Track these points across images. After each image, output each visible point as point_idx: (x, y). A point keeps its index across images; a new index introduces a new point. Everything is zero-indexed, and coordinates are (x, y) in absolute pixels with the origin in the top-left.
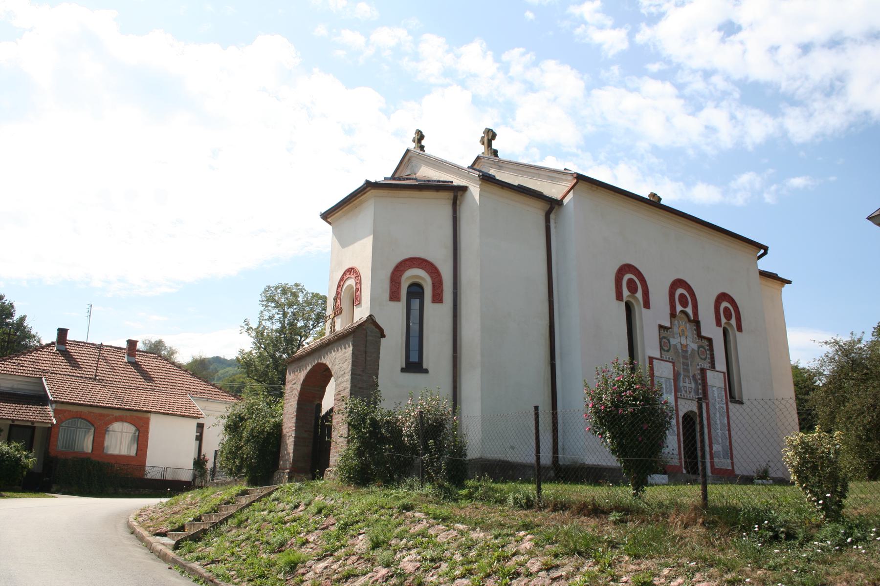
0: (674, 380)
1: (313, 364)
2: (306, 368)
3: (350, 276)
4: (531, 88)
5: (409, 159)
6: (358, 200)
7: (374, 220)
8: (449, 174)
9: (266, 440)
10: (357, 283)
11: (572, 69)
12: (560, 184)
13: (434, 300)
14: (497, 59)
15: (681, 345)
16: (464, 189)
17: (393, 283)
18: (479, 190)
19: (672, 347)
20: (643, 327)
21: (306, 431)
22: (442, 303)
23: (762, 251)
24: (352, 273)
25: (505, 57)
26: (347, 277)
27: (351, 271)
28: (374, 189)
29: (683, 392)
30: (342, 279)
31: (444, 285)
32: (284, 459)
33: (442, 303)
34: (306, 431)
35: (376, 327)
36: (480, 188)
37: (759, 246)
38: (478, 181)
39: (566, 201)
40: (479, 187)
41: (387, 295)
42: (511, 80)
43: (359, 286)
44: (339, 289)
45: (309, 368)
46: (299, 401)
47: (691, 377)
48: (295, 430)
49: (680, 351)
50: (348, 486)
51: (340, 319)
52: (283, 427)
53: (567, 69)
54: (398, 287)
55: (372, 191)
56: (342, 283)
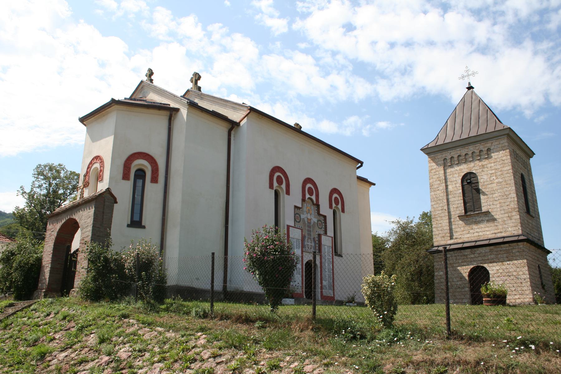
0: (301, 240)
1: (67, 219)
2: (61, 222)
6: (101, 114)
9: (30, 269)
10: (101, 167)
15: (307, 219)
16: (177, 110)
18: (187, 111)
19: (301, 220)
21: (59, 264)
22: (157, 183)
23: (360, 164)
29: (307, 248)
30: (91, 163)
32: (42, 282)
34: (59, 264)
37: (358, 161)
39: (242, 123)
41: (121, 176)
43: (102, 168)
44: (89, 169)
45: (63, 221)
46: (55, 243)
47: (312, 240)
49: (307, 223)
51: (88, 190)
52: (43, 261)
55: (116, 106)
56: (91, 166)
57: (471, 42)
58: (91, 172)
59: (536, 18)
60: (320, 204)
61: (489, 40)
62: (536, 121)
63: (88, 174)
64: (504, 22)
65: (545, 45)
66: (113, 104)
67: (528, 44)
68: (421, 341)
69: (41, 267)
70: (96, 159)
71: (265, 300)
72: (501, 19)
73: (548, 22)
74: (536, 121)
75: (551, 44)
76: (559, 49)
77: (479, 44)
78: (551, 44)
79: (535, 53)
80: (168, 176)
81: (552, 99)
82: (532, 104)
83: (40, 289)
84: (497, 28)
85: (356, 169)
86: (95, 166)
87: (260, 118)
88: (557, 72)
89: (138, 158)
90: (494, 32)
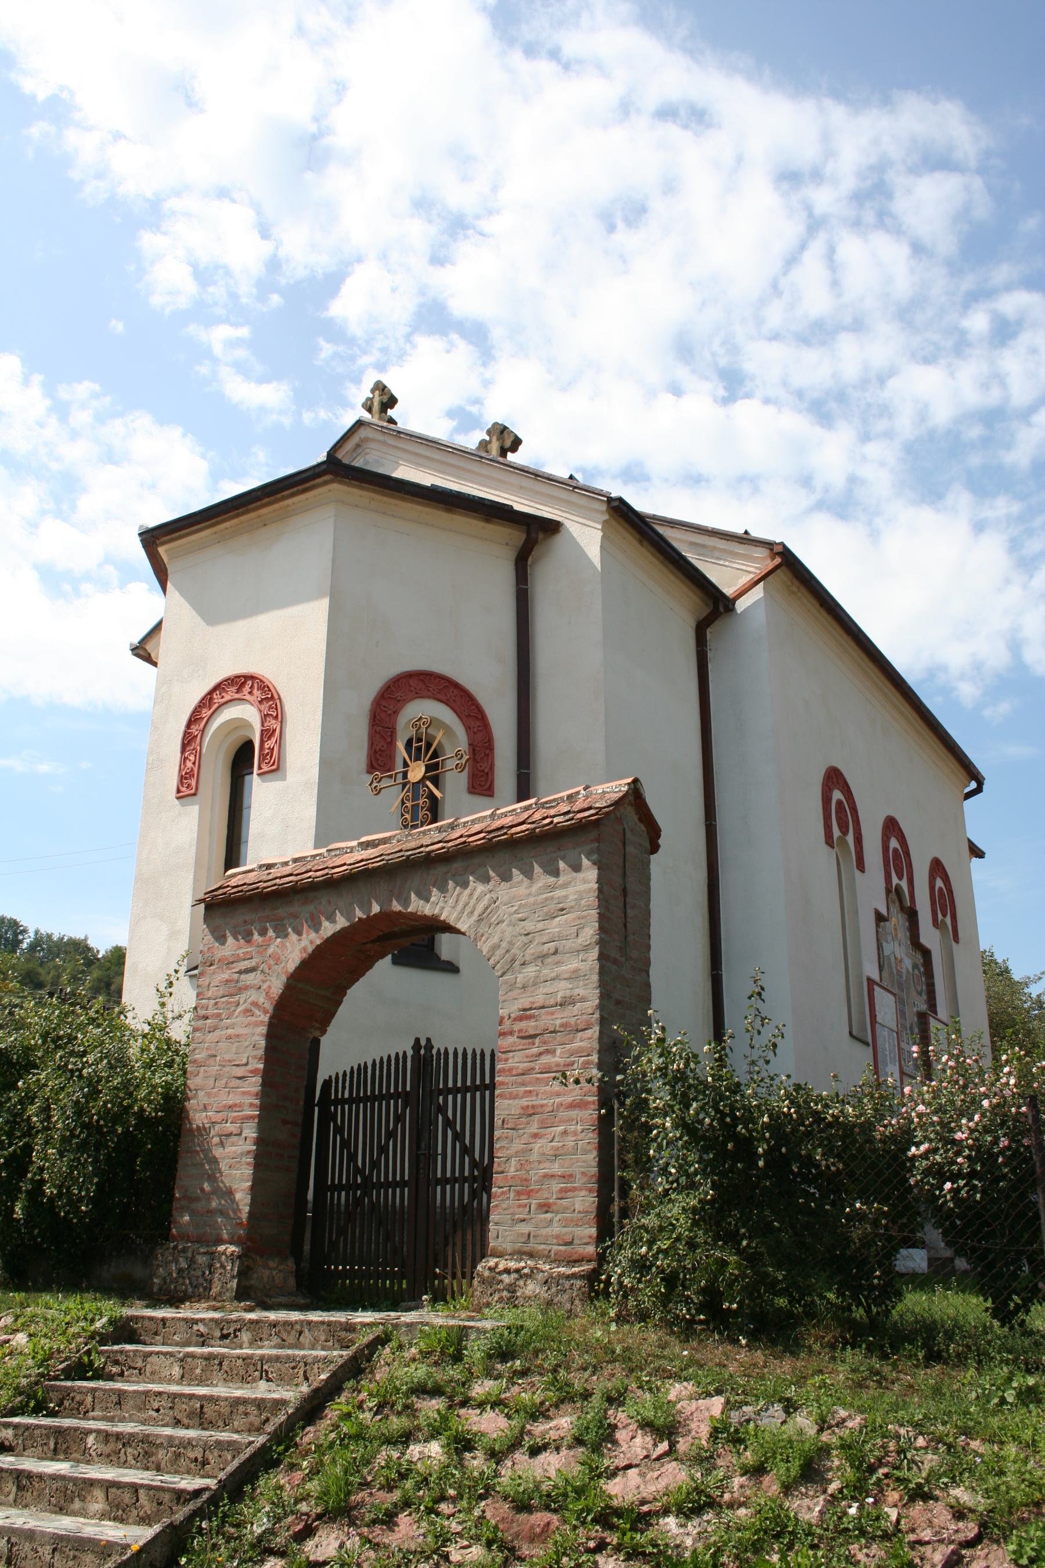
1: (359, 914)
2: (316, 927)
3: (237, 696)
4: (111, 457)
5: (358, 446)
6: (276, 506)
7: (334, 560)
8: (496, 489)
9: (129, 1144)
10: (264, 718)
11: (185, 435)
12: (727, 563)
13: (473, 787)
14: (49, 390)
16: (552, 527)
17: (378, 729)
18: (600, 534)
20: (857, 912)
21: (285, 1122)
22: (492, 796)
23: (973, 785)
24: (247, 689)
25: (64, 393)
26: (227, 697)
27: (244, 684)
28: (341, 483)
30: (207, 701)
31: (496, 751)
32: (199, 1206)
33: (492, 796)
34: (285, 1122)
35: (640, 820)
36: (602, 530)
37: (972, 773)
38: (602, 512)
39: (741, 605)
40: (600, 527)
41: (360, 756)
42: (75, 435)
43: (272, 723)
44: (195, 729)
45: (328, 929)
46: (271, 1025)
48: (259, 1116)
50: (833, 1359)
51: (196, 808)
52: (191, 1104)
53: (175, 432)
54: (389, 740)
55: (335, 486)
56: (206, 713)
57: (806, 481)
58: (207, 740)
59: (975, 432)
60: (918, 908)
61: (853, 480)
62: (987, 713)
63: (195, 744)
64: (889, 435)
65: (1002, 507)
66: (327, 477)
67: (961, 499)
68: (187, 1367)
69: (177, 1137)
70: (234, 689)
71: (746, 1267)
72: (881, 425)
73: (1009, 446)
74: (987, 713)
75: (1016, 508)
76: (1038, 522)
77: (826, 490)
78: (1016, 508)
79: (979, 527)
80: (531, 771)
81: (1030, 655)
82: (978, 666)
83: (185, 1237)
84: (872, 449)
85: (962, 798)
86: (229, 714)
87: (792, 593)
88: (1037, 582)
89: (418, 695)
90: (864, 458)
